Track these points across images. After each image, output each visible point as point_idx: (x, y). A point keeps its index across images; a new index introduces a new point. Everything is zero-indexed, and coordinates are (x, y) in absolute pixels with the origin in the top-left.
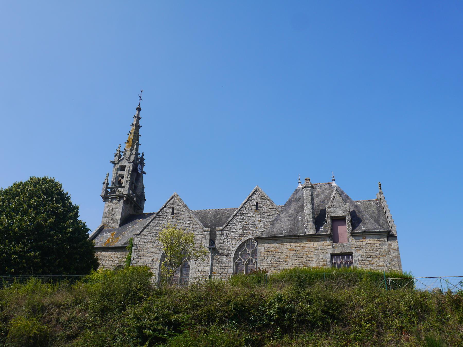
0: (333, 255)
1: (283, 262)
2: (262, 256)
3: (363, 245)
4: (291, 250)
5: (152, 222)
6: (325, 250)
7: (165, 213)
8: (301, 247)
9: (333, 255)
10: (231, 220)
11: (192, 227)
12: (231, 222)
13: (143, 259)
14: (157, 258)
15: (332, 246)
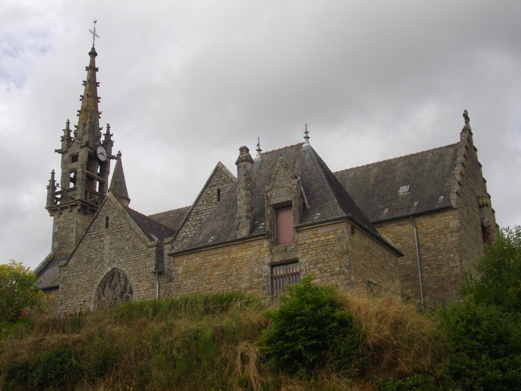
0: (273, 265)
1: (206, 286)
2: (180, 281)
3: (313, 243)
4: (217, 266)
5: (81, 245)
6: (261, 260)
7: (97, 228)
8: (230, 259)
9: (273, 265)
10: (184, 224)
11: (132, 243)
12: (184, 228)
13: (73, 302)
14: (90, 298)
15: (271, 251)
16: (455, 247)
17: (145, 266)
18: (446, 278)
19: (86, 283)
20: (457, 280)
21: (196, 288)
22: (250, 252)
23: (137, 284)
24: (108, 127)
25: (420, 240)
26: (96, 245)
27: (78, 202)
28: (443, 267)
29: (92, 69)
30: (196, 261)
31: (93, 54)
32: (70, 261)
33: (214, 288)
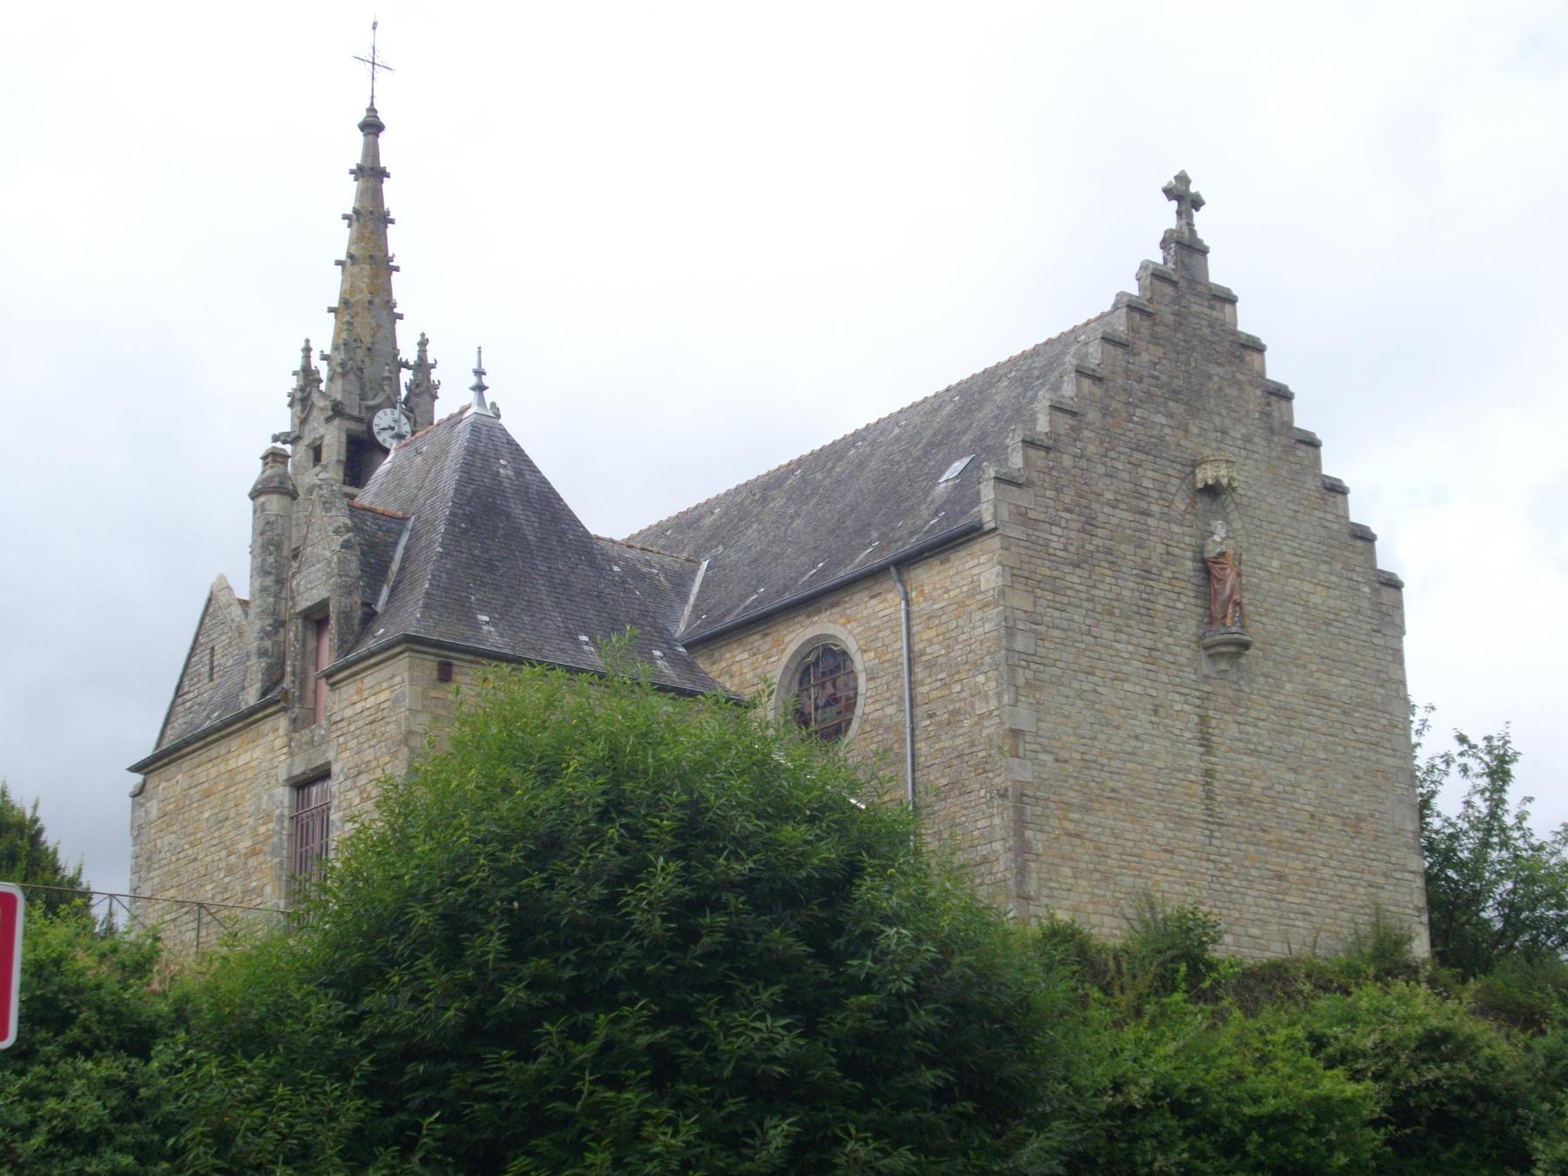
16: (989, 653)
18: (966, 752)
20: (990, 756)
22: (258, 753)
24: (423, 343)
25: (916, 638)
28: (961, 718)
29: (371, 173)
31: (372, 127)
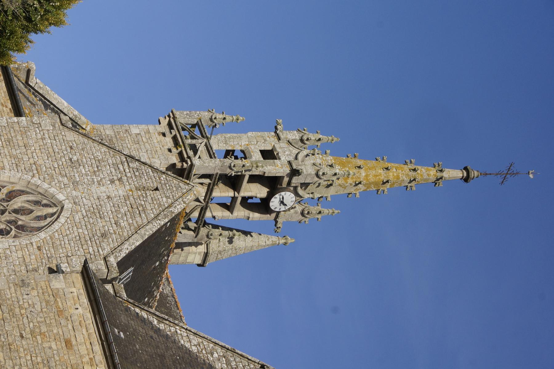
11: (112, 231)
17: (69, 254)
19: (32, 161)
21: (23, 311)
23: (34, 244)
26: (105, 173)
27: (189, 163)
30: (77, 309)
32: (72, 133)
33: (24, 343)
